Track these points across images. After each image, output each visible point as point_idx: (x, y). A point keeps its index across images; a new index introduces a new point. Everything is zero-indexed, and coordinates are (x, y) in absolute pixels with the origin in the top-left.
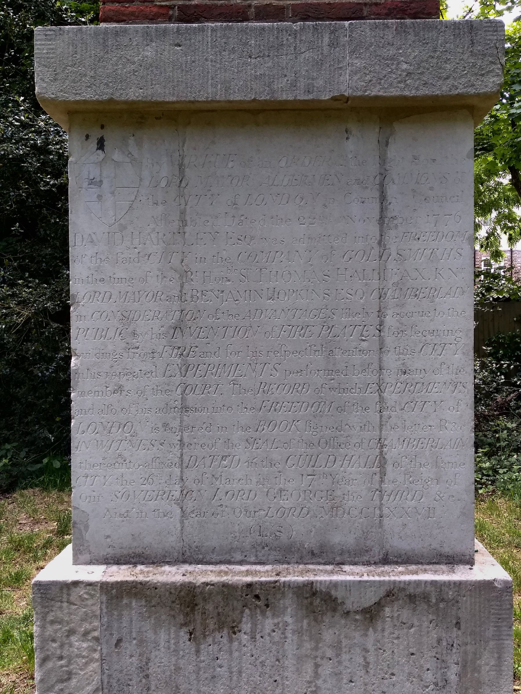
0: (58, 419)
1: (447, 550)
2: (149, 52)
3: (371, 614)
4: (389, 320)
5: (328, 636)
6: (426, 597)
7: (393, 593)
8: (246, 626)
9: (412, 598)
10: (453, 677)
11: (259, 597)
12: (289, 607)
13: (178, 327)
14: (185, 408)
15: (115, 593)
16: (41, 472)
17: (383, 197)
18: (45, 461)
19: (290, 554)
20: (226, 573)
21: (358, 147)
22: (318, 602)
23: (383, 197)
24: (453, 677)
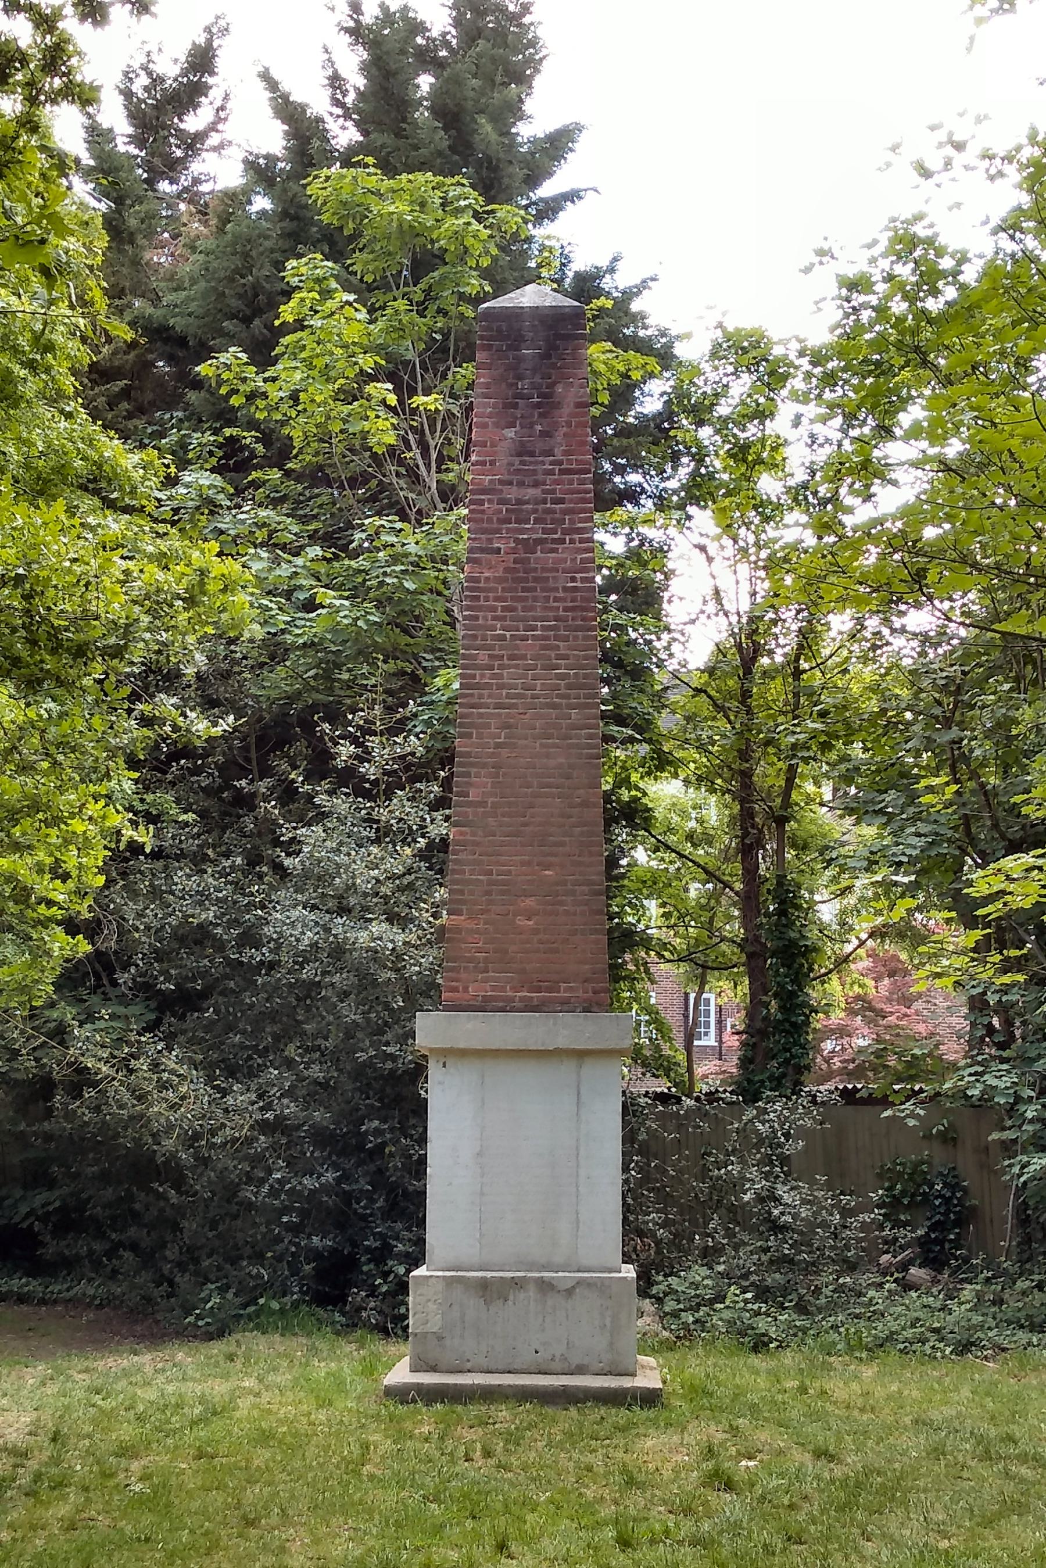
0: (269, 1254)
1: (609, 1265)
2: (469, 1026)
3: (570, 1292)
4: (582, 1152)
5: (550, 1302)
6: (595, 1285)
7: (580, 1282)
8: (511, 1297)
9: (589, 1285)
10: (608, 1324)
11: (517, 1284)
12: (532, 1291)
13: (479, 1154)
14: (482, 1194)
15: (450, 1282)
16: (258, 1314)
17: (579, 1093)
18: (262, 1301)
19: (531, 1267)
20: (548, 855)
21: (567, 1069)
22: (545, 1287)
23: (579, 1093)
24: (608, 1324)
